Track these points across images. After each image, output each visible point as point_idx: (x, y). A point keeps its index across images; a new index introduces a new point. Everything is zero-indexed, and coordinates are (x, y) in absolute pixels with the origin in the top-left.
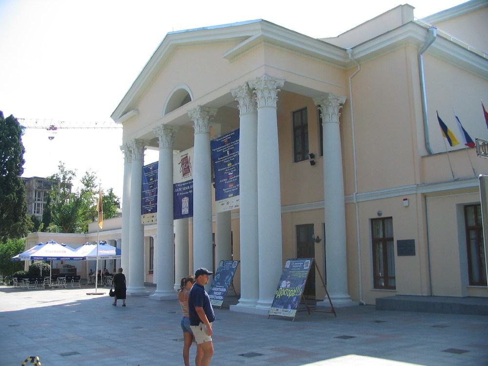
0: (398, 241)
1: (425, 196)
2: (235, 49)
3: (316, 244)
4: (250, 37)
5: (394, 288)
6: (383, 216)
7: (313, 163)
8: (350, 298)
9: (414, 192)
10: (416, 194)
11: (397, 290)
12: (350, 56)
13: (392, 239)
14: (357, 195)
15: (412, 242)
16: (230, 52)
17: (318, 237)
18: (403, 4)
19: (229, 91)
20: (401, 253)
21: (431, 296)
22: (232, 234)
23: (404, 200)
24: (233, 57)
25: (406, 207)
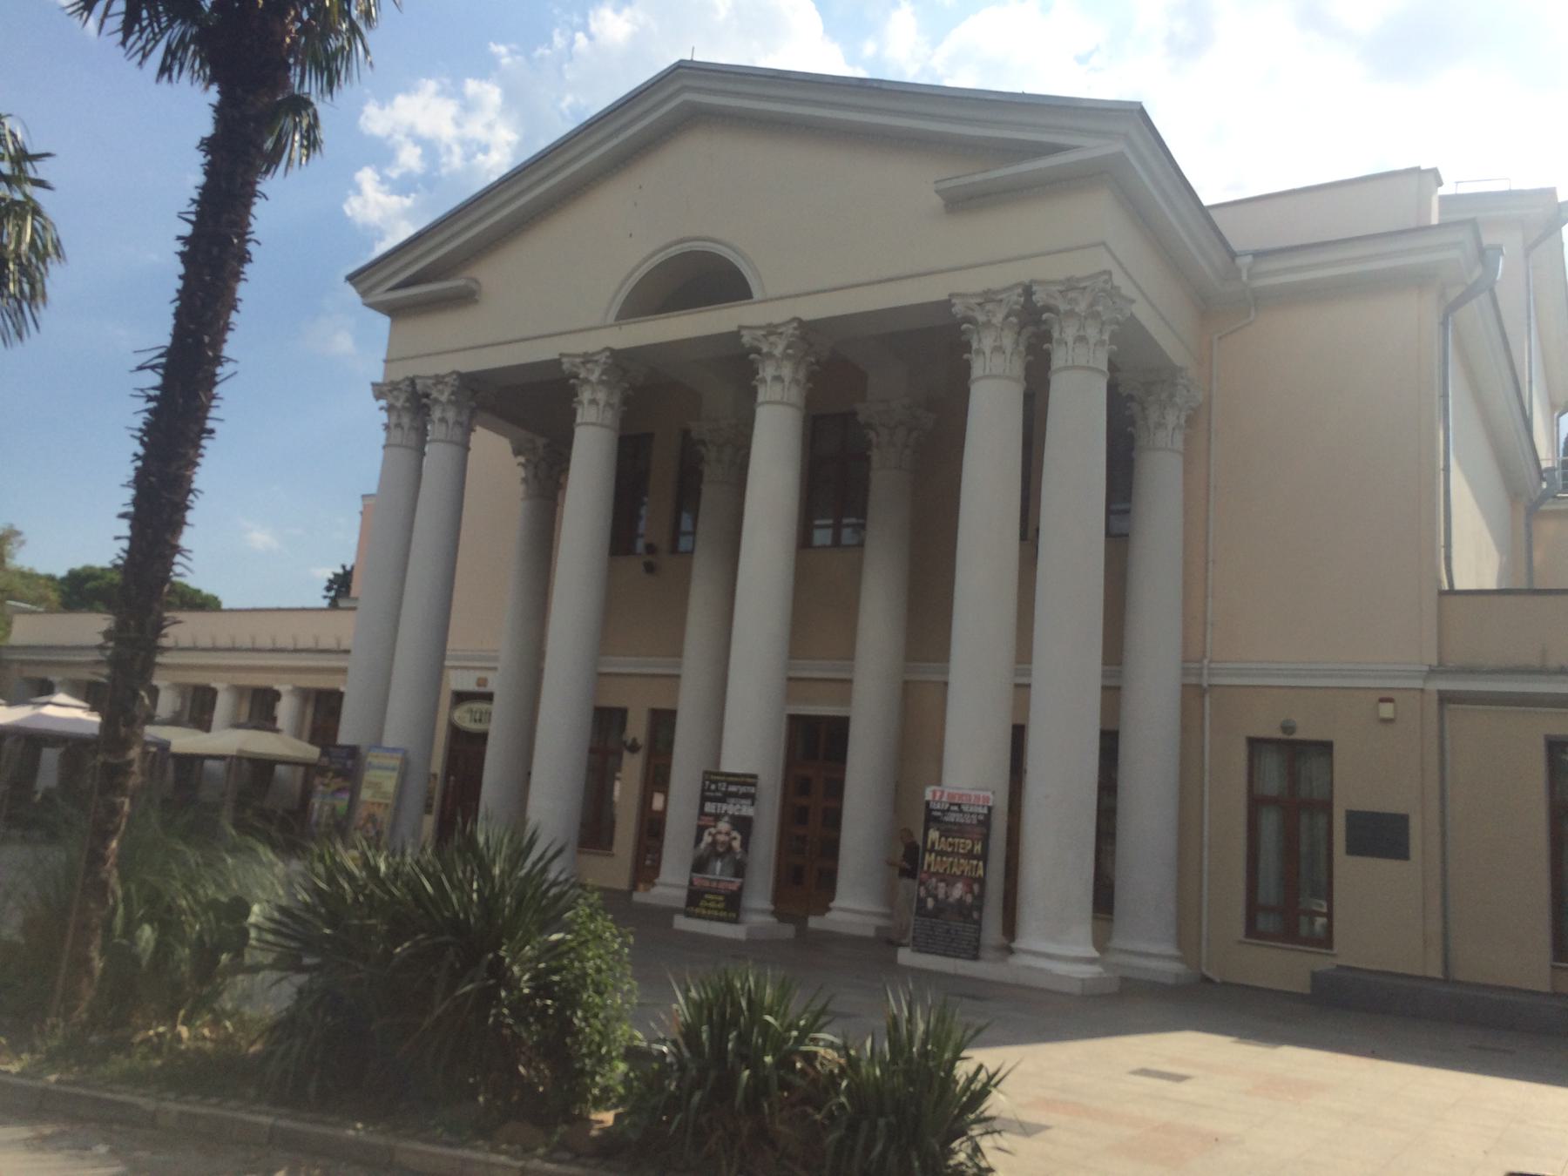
0: (1353, 817)
1: (1445, 698)
2: (978, 178)
3: (626, 754)
4: (1056, 149)
5: (1326, 941)
6: (1298, 736)
7: (650, 568)
8: (884, 915)
9: (1418, 684)
10: (1422, 690)
11: (1335, 951)
12: (1244, 277)
13: (1327, 806)
14: (1213, 665)
15: (1347, 811)
16: (967, 180)
17: (634, 740)
18: (1423, 168)
19: (557, 357)
20: (1357, 847)
21: (1446, 981)
22: (1019, 734)
23: (1382, 700)
24: (960, 202)
25: (1387, 721)
